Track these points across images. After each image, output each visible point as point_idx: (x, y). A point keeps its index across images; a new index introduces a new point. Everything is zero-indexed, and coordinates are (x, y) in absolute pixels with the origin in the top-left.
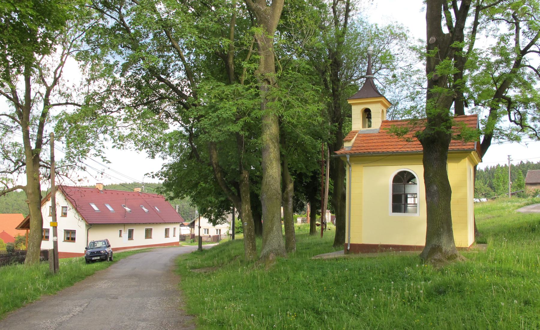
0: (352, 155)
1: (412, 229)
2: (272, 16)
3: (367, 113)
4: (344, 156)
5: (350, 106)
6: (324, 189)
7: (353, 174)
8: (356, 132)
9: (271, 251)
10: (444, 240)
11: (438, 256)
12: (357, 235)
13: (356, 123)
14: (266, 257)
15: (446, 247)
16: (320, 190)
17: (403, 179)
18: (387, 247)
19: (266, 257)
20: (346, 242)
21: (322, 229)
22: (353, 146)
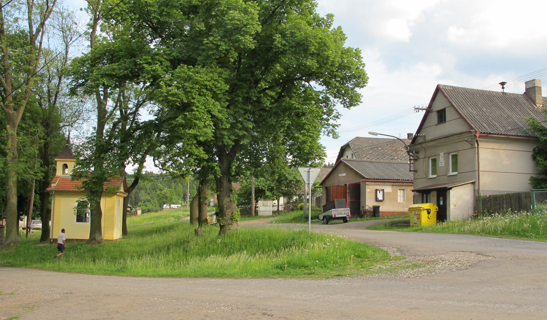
0: (56, 192)
1: (83, 231)
2: (17, 117)
3: (65, 166)
4: (51, 191)
5: (56, 161)
6: (30, 201)
7: (56, 201)
8: (58, 177)
9: (12, 242)
10: (97, 235)
11: (94, 242)
12: (56, 234)
13: (59, 173)
14: (9, 244)
15: (98, 238)
16: (27, 202)
17: (82, 206)
18: (73, 240)
19: (9, 244)
20: (51, 237)
21: (27, 232)
22: (56, 186)
